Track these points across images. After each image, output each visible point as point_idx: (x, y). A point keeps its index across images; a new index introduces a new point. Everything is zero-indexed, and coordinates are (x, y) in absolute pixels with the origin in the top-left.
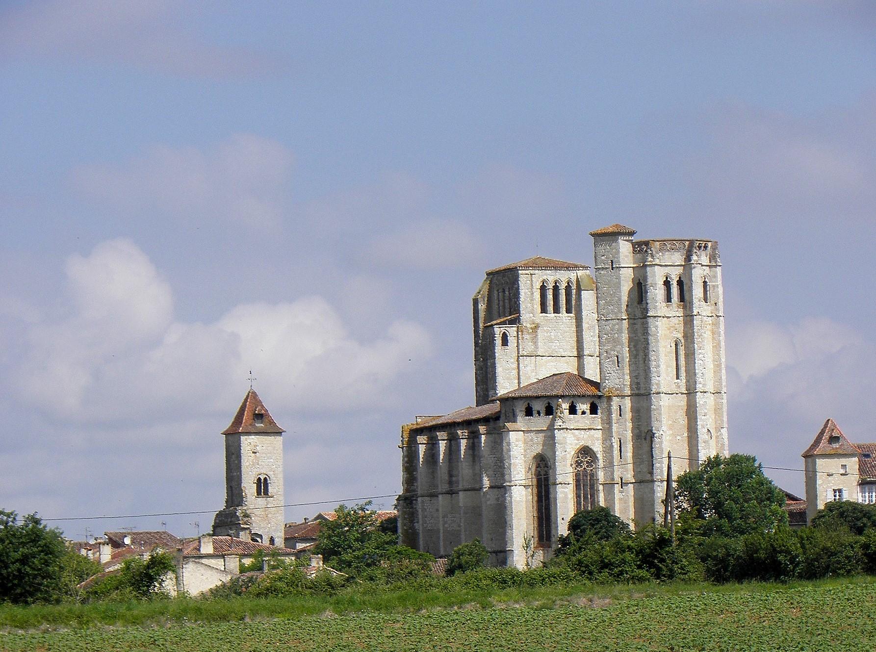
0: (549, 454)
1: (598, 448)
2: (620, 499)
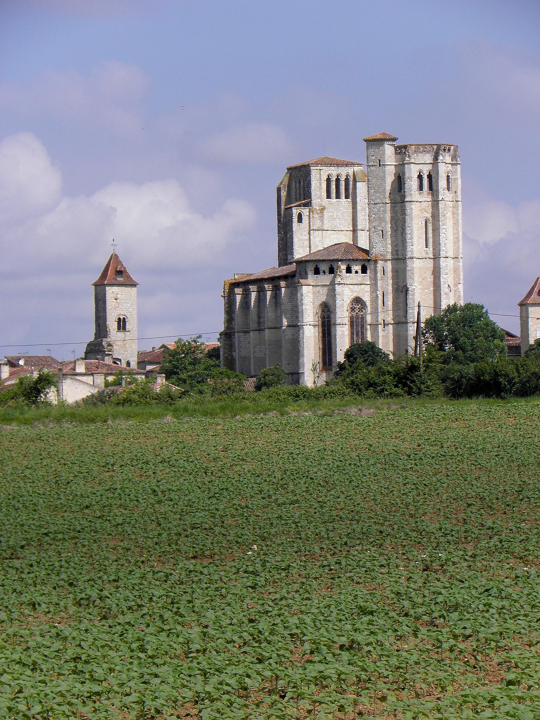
0: (331, 303)
1: (367, 298)
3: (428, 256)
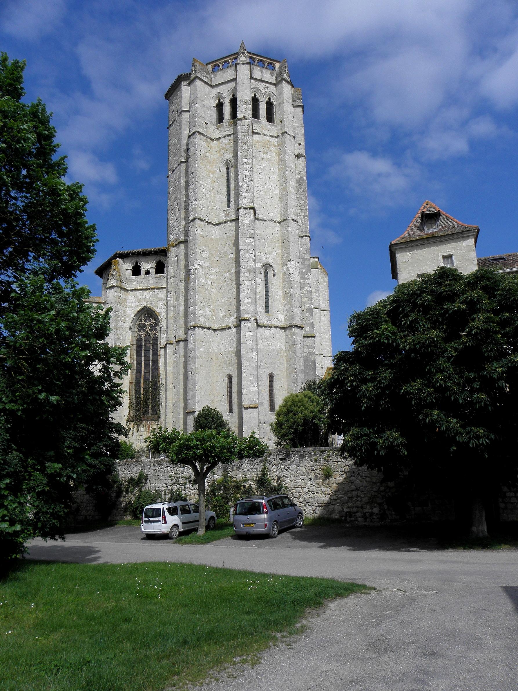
1: (160, 309)
3: (230, 219)
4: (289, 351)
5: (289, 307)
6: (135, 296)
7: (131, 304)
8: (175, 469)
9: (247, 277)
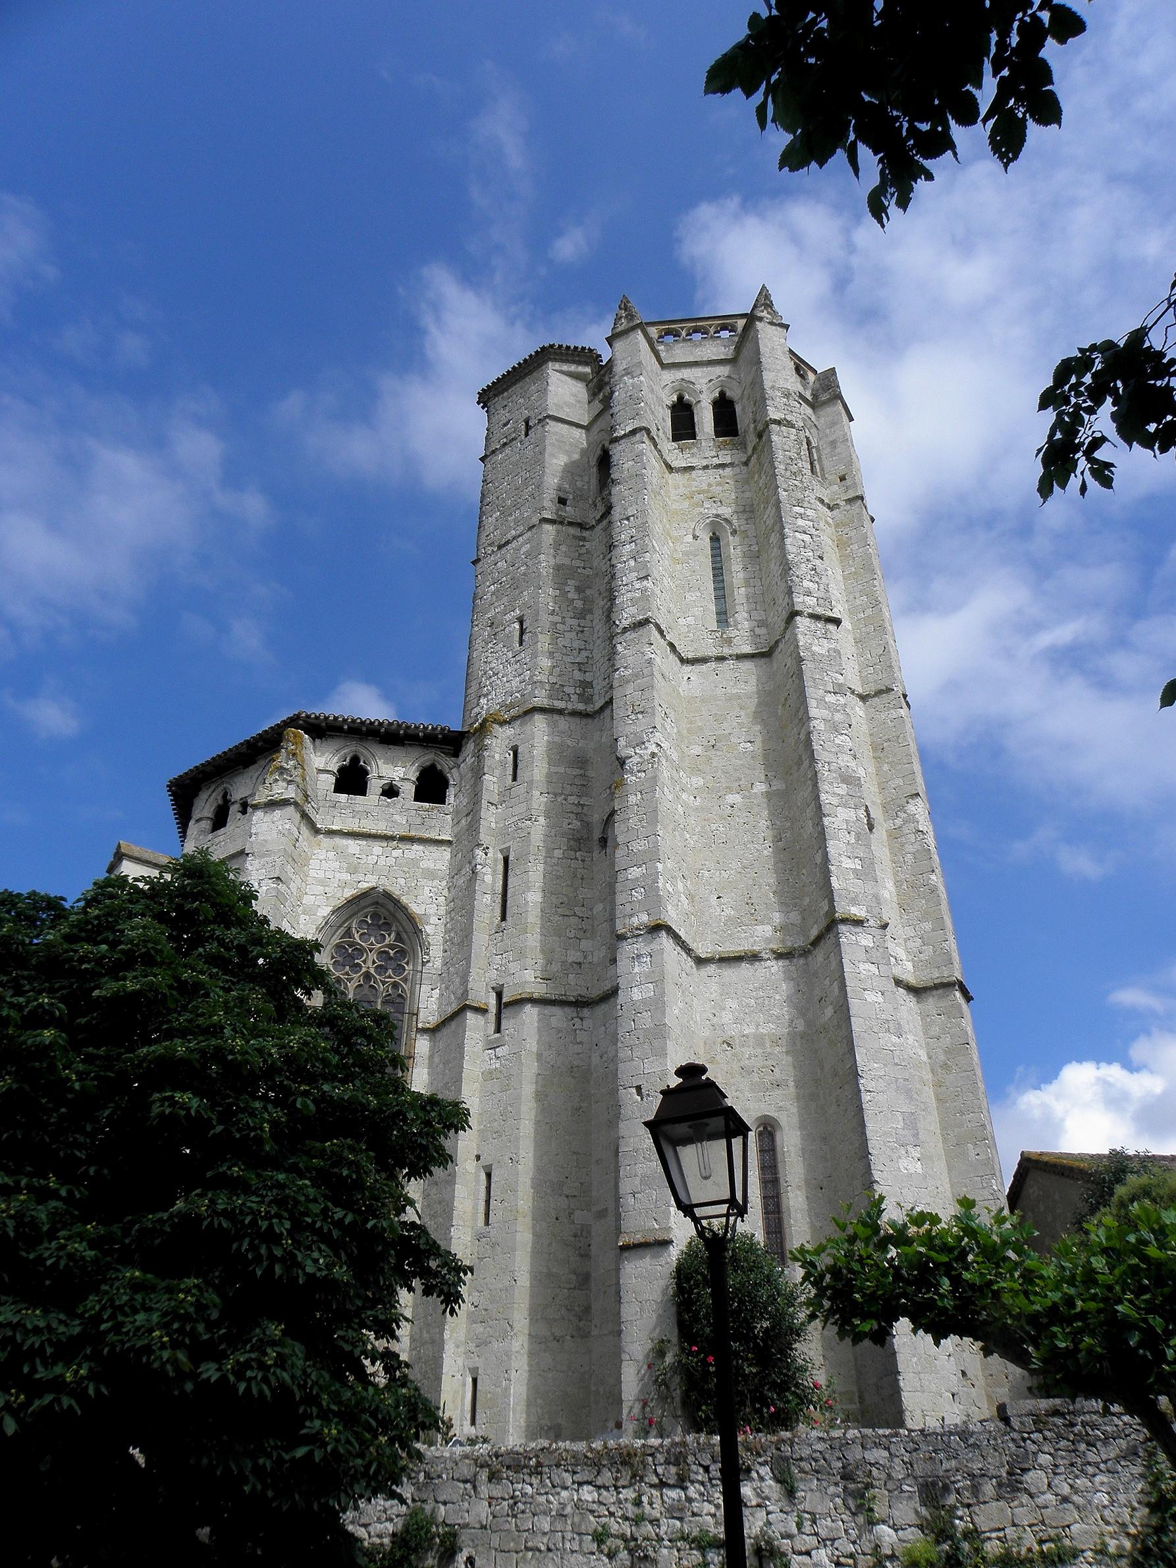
1: (428, 903)
2: (489, 1075)
4: (945, 1066)
5: (927, 926)
6: (340, 853)
7: (321, 875)
8: (629, 1494)
9: (842, 796)
